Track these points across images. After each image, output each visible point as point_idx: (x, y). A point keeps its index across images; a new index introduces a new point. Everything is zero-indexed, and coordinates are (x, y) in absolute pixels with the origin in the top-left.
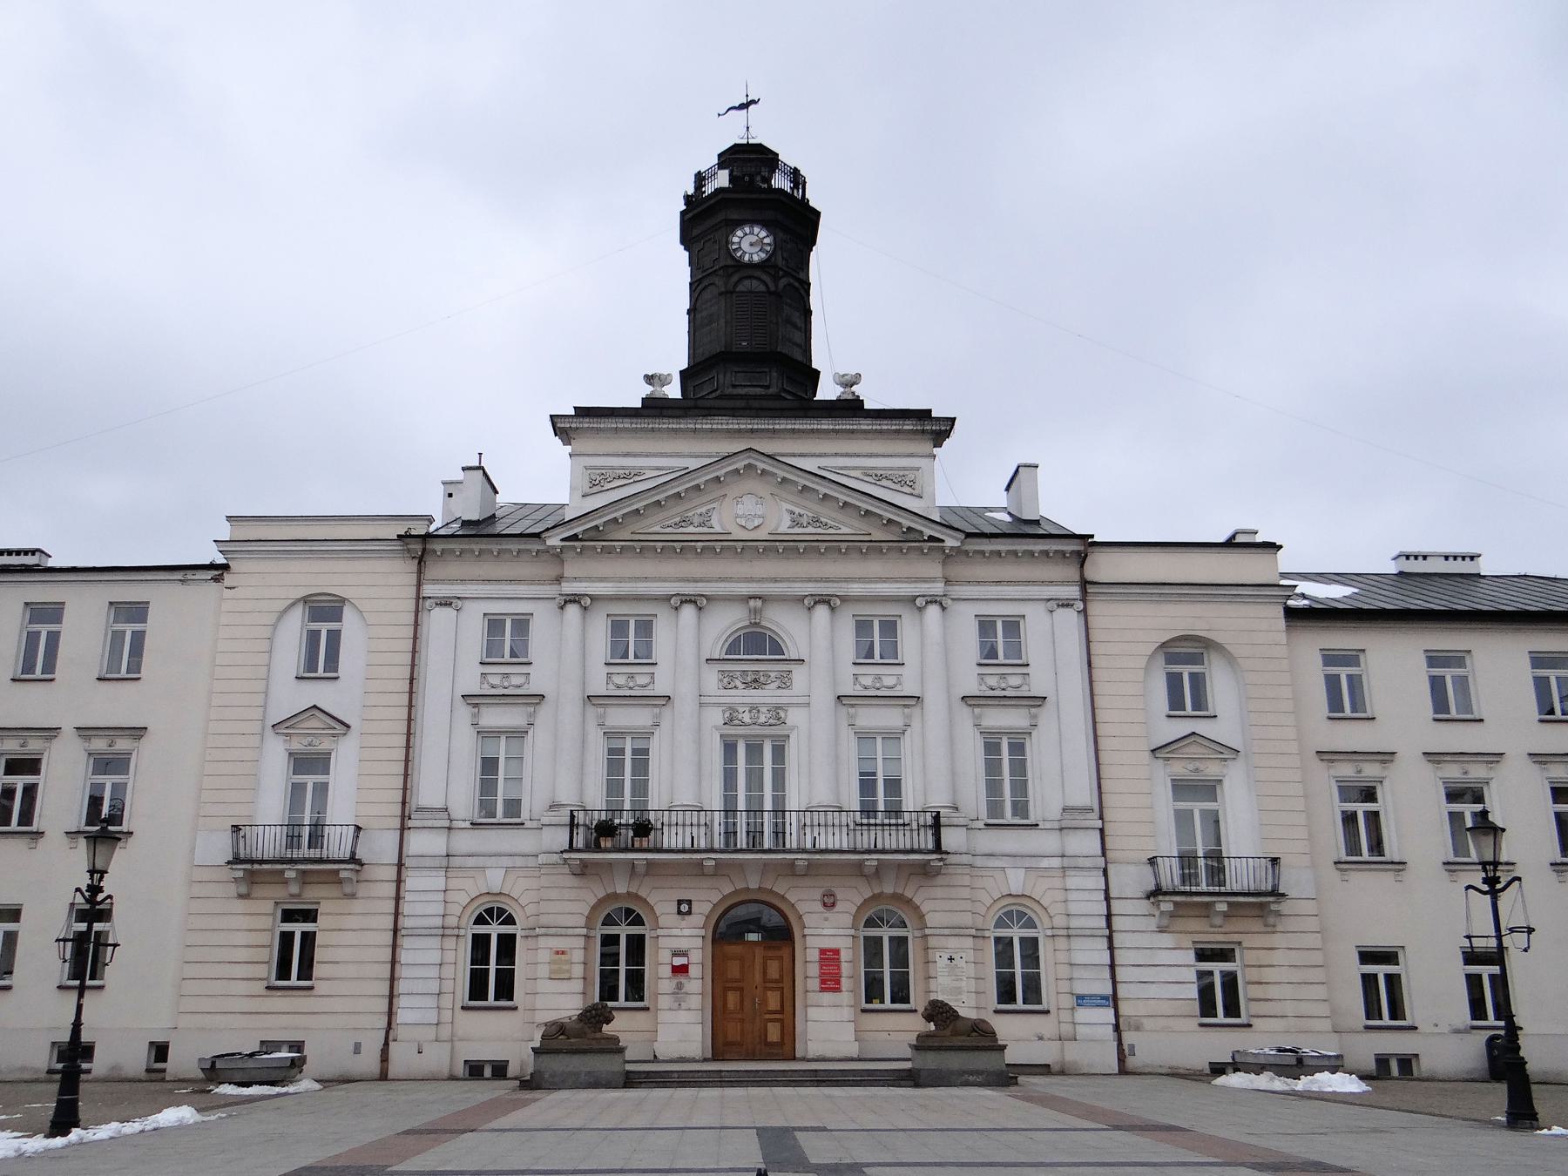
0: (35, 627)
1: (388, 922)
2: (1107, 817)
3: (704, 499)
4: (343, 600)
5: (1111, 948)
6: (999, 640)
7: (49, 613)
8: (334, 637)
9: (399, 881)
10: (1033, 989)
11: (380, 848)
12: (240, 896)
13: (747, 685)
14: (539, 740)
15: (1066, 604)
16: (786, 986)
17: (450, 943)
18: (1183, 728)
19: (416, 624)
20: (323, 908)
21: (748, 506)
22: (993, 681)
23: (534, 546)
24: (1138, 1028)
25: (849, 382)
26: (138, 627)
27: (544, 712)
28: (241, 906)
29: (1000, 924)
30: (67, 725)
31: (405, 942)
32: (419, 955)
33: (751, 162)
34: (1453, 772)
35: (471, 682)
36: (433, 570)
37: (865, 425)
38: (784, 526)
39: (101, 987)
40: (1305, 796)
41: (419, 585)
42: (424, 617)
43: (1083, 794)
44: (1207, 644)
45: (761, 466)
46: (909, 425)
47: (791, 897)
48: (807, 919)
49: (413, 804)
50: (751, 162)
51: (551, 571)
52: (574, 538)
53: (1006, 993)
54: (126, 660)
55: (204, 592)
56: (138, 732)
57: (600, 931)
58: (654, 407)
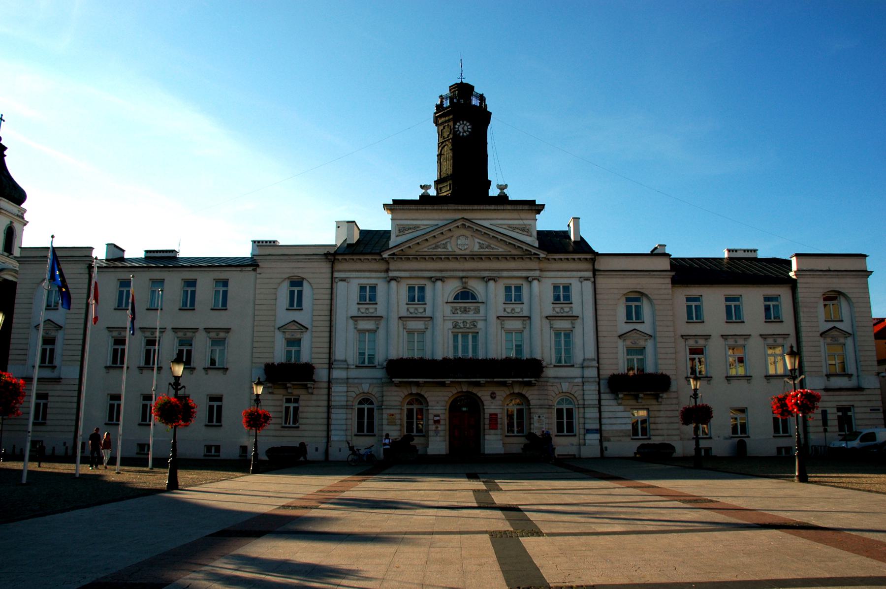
0: (122, 289)
1: (325, 403)
2: (601, 361)
3: (445, 237)
4: (303, 279)
5: (600, 412)
6: (562, 294)
7: (192, 283)
8: (300, 293)
9: (329, 388)
10: (570, 428)
11: (321, 374)
12: (270, 393)
13: (462, 312)
14: (381, 333)
15: (587, 279)
17: (349, 411)
18: (631, 327)
19: (332, 288)
20: (302, 397)
22: (558, 310)
24: (609, 440)
25: (502, 188)
26: (193, 289)
31: (333, 411)
32: (338, 416)
33: (463, 91)
34: (691, 342)
35: (354, 311)
36: (338, 266)
37: (509, 207)
38: (476, 248)
39: (221, 426)
40: (675, 353)
41: (332, 273)
42: (335, 285)
43: (591, 353)
44: (840, 293)
46: (526, 207)
47: (479, 394)
48: (485, 403)
49: (333, 358)
50: (463, 91)
51: (383, 266)
52: (394, 254)
53: (560, 428)
54: (222, 304)
55: (248, 275)
56: (228, 330)
57: (405, 407)
58: (425, 199)
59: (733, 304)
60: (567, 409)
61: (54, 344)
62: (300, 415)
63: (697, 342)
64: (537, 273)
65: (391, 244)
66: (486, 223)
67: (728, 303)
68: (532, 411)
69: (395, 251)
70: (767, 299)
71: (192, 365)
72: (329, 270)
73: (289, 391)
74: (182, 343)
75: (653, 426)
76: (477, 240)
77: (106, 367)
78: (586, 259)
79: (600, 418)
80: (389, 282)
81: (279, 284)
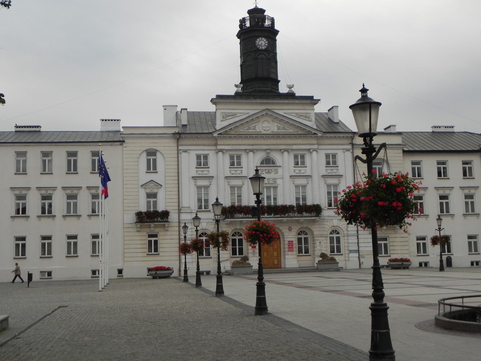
4: (157, 151)
8: (155, 161)
11: (173, 217)
12: (138, 231)
15: (348, 150)
16: (279, 250)
19: (178, 157)
20: (160, 233)
21: (266, 124)
23: (210, 136)
24: (364, 257)
25: (290, 87)
26: (75, 158)
27: (214, 182)
28: (137, 234)
29: (331, 233)
30: (33, 186)
34: (466, 191)
36: (181, 142)
37: (297, 101)
38: (275, 130)
41: (178, 146)
42: (180, 155)
45: (270, 113)
47: (281, 228)
48: (285, 234)
51: (213, 142)
52: (221, 134)
59: (467, 166)
60: (154, 241)
61: (447, 199)
62: (159, 246)
63: (470, 191)
64: (316, 147)
65: (218, 127)
66: (281, 112)
67: (439, 166)
68: (316, 238)
69: (221, 132)
70: (464, 163)
71: (53, 214)
72: (176, 145)
73: (152, 229)
74: (44, 198)
75: (392, 248)
76: (276, 124)
77: (12, 217)
78: (348, 137)
79: (358, 243)
80: (217, 153)
81: (141, 154)
